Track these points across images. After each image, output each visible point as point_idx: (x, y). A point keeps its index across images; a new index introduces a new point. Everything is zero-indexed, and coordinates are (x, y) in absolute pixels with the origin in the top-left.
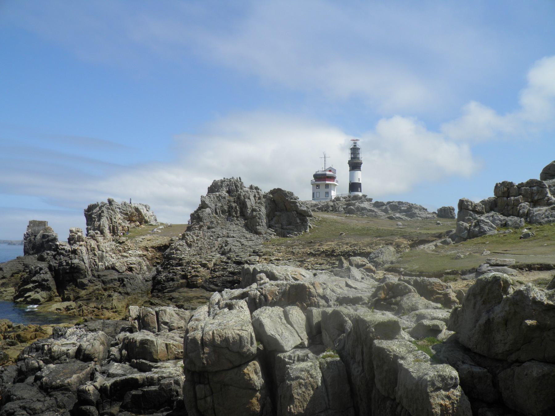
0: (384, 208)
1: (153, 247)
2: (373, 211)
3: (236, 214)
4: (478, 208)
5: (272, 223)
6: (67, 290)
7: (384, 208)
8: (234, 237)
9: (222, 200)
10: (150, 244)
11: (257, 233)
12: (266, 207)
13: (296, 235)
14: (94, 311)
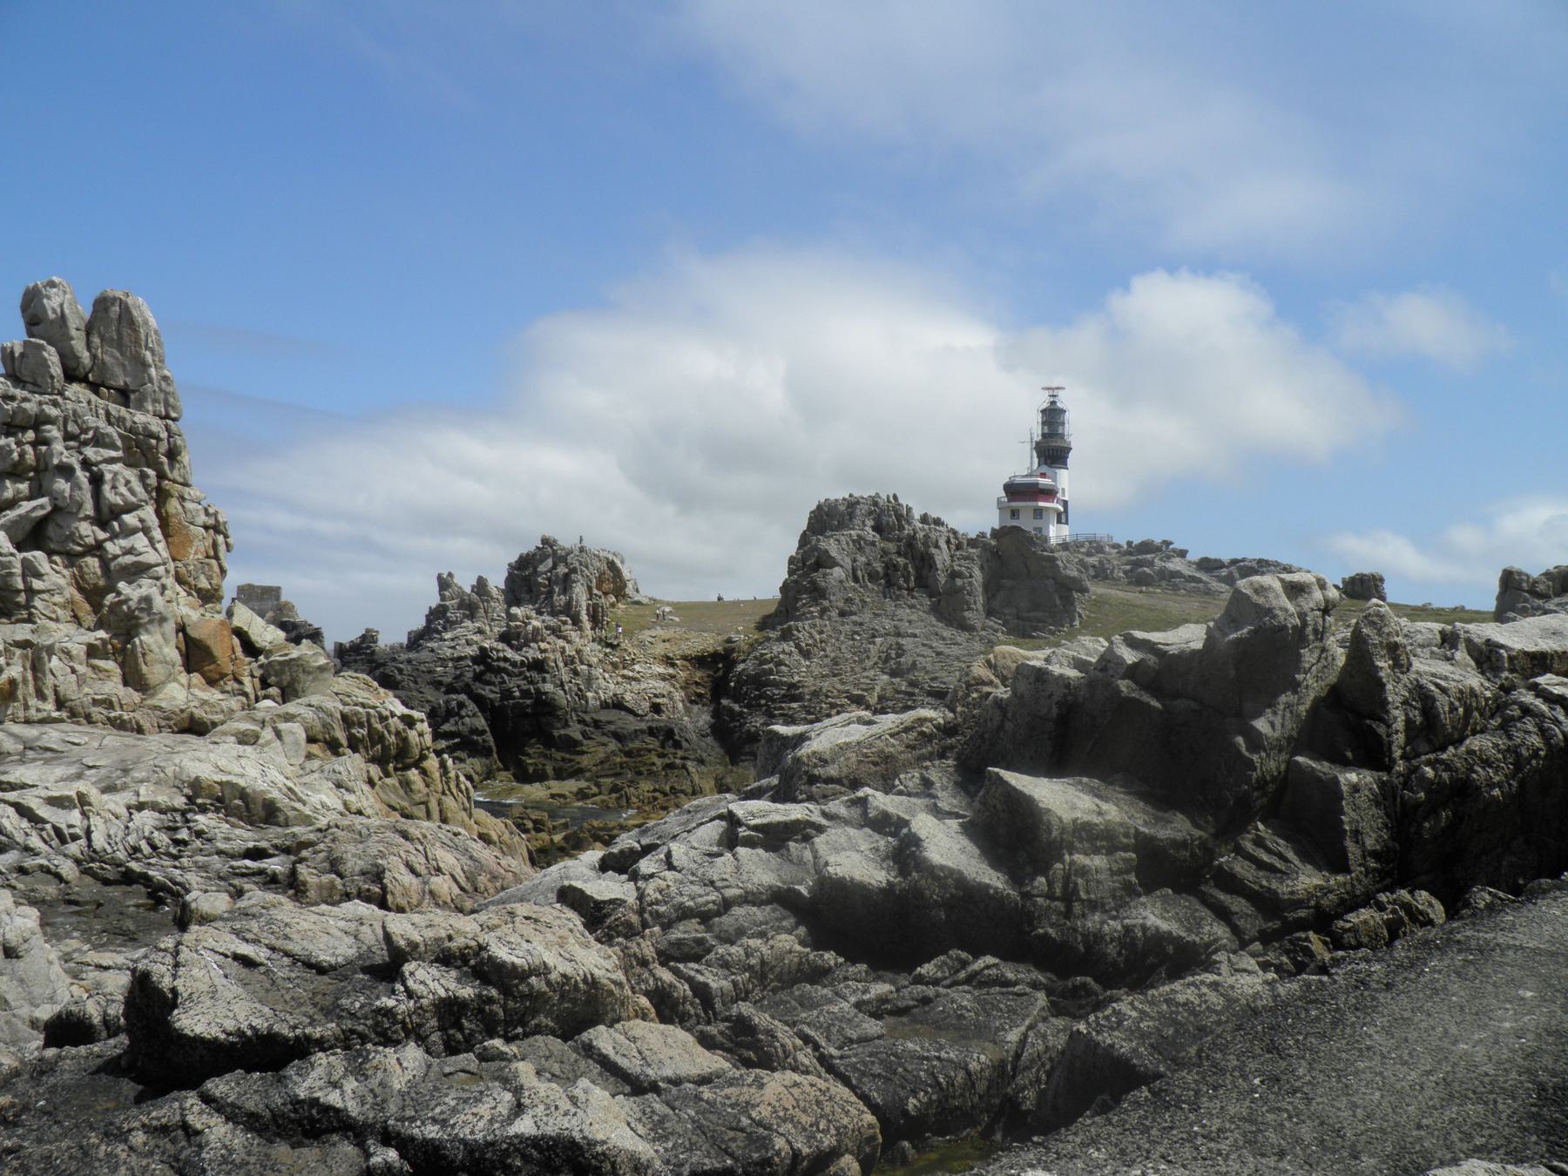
0: (1224, 572)
1: (685, 658)
2: (1199, 581)
3: (907, 581)
4: (1541, 588)
5: (996, 604)
6: (528, 755)
7: (1224, 572)
8: (915, 636)
9: (867, 549)
10: (675, 651)
11: (964, 626)
12: (982, 568)
13: (1053, 633)
14: (655, 799)
